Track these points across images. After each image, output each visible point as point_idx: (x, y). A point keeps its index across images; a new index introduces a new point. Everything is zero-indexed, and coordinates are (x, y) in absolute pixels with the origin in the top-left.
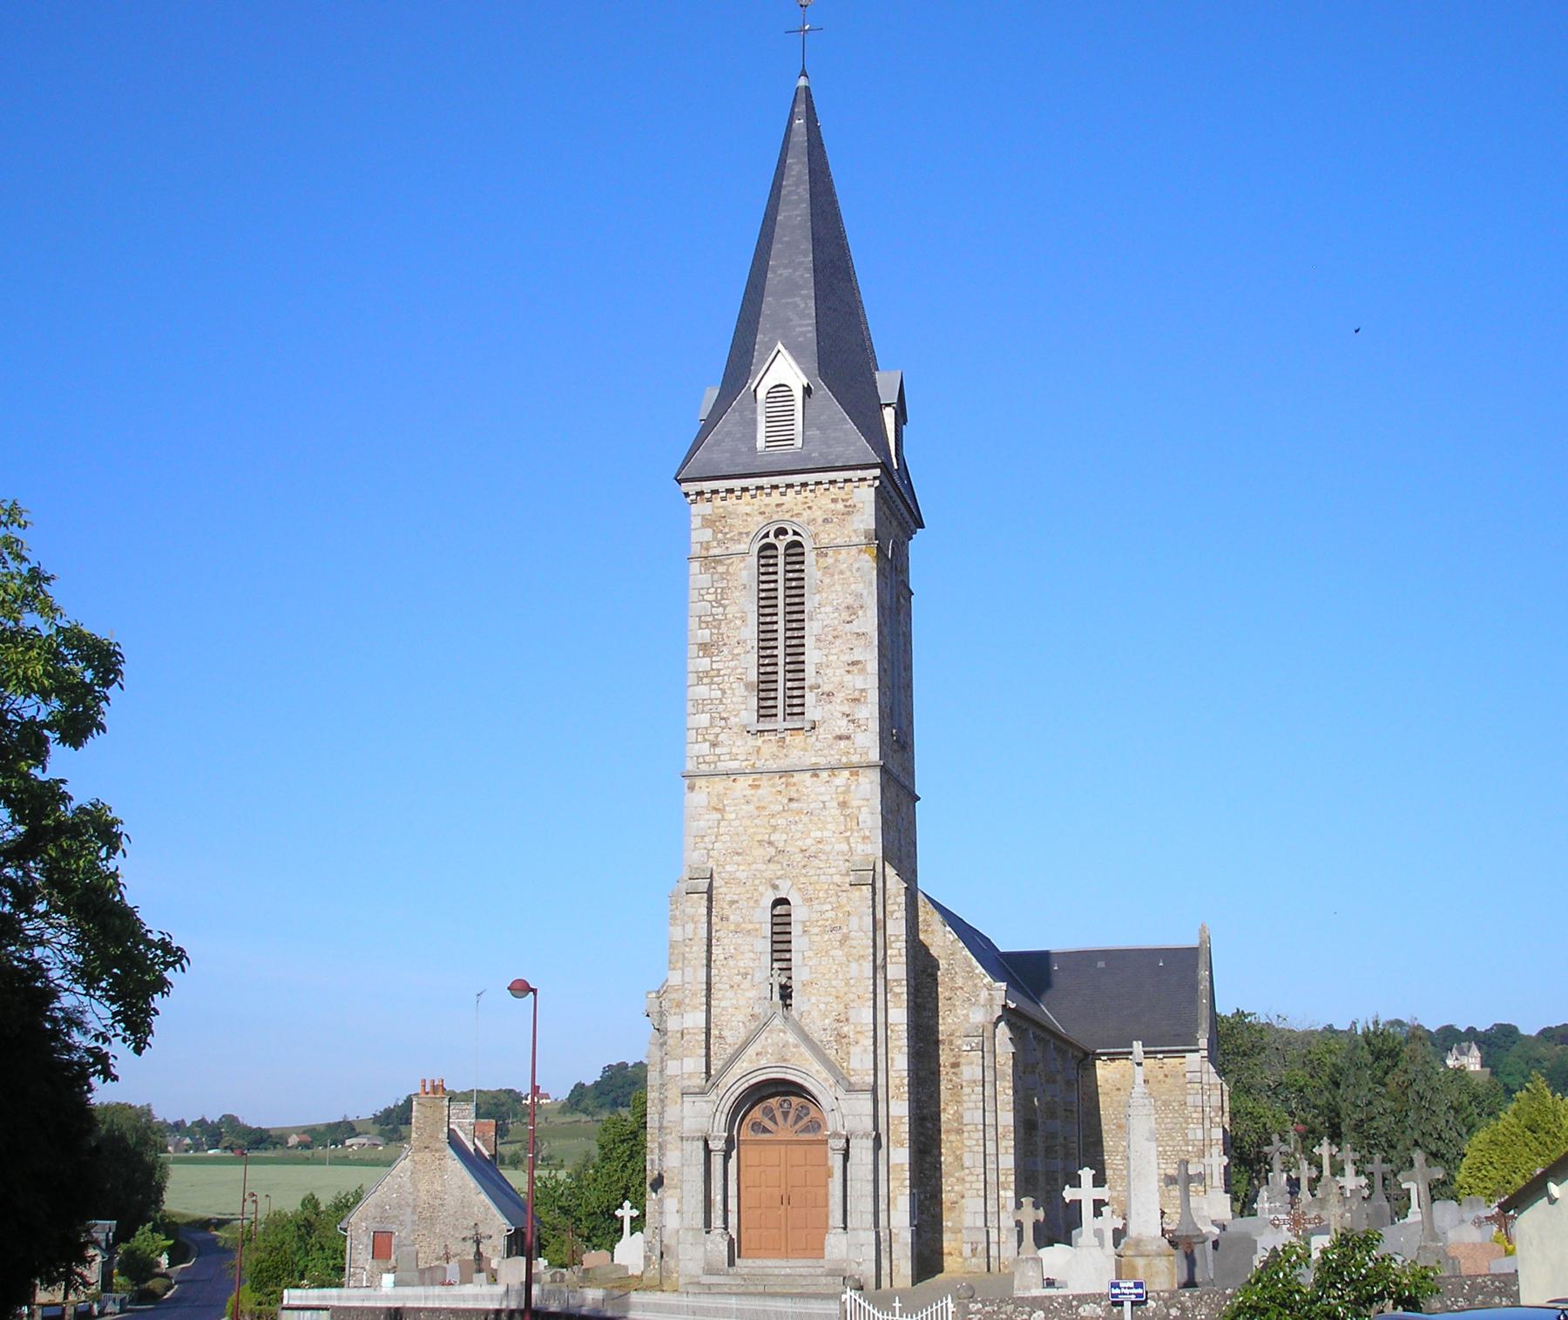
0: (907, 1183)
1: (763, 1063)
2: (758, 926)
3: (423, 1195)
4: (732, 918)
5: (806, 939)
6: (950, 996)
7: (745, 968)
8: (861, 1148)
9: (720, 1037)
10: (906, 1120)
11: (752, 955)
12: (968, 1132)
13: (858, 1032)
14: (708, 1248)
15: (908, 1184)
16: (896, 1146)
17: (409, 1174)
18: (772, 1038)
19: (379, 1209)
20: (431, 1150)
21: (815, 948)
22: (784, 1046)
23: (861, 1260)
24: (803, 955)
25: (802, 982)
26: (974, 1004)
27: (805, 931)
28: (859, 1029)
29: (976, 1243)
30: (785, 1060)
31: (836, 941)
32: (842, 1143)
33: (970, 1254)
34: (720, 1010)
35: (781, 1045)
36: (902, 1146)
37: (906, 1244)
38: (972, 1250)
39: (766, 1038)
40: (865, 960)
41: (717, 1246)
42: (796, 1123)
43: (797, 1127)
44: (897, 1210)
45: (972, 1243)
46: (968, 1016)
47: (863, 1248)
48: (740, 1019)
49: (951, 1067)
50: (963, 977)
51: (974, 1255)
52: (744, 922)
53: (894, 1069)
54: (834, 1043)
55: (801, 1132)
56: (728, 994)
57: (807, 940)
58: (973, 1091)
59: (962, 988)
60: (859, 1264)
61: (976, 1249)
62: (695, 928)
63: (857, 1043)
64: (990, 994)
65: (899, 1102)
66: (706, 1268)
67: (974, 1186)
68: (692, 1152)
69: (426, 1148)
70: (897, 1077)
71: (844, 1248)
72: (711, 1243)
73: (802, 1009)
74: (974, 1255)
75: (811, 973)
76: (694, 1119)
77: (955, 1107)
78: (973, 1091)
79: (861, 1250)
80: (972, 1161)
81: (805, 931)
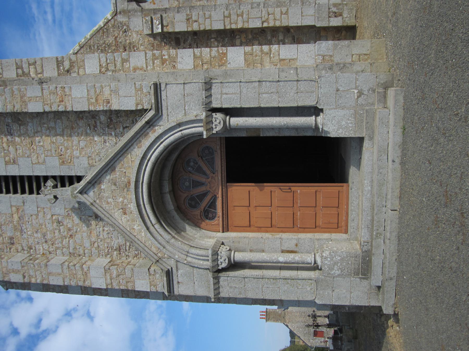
0: (266, 48)
1: (133, 206)
2: (14, 209)
3: (301, 319)
4: (9, 234)
5: (21, 161)
6: (122, 48)
7: (53, 223)
8: (222, 94)
9: (119, 251)
10: (197, 51)
11: (41, 215)
12: (231, 24)
13: (97, 100)
14: (338, 272)
15: (268, 46)
16: (226, 61)
17: (293, 324)
18: (108, 197)
19: (306, 335)
20: (285, 316)
21: (28, 152)
22: (115, 184)
23: (356, 91)
24: (36, 164)
25: (61, 165)
26: (128, 27)
27: (14, 162)
28: (93, 101)
29: (329, 13)
30: (129, 183)
31: (20, 130)
32: (219, 116)
33: (340, 18)
34: (93, 249)
35: (113, 187)
36: (225, 54)
37: (335, 47)
38: (335, 16)
39: (108, 203)
40: (25, 95)
41: (336, 263)
42: (205, 174)
43: (208, 172)
44: (297, 59)
45: (330, 17)
46: (137, 32)
47: (341, 89)
48: (101, 229)
49: (175, 37)
50: (108, 37)
51: (341, 15)
52: (12, 222)
53: (145, 66)
54: (118, 130)
55: (213, 169)
56: (78, 241)
57: (21, 159)
58: (196, 21)
59: (116, 37)
60: (360, 94)
61: (335, 13)
62: (13, 271)
63: (109, 102)
64: (120, 13)
65: (179, 59)
66: (360, 276)
67: (278, 17)
68: (231, 287)
69: (284, 318)
70: (154, 63)
71: (341, 113)
72: (333, 269)
73: (86, 165)
74: (341, 15)
75: (52, 156)
76: (196, 283)
77: (212, 40)
78: (196, 21)
79: (343, 91)
80: (257, 20)
81: (14, 162)
